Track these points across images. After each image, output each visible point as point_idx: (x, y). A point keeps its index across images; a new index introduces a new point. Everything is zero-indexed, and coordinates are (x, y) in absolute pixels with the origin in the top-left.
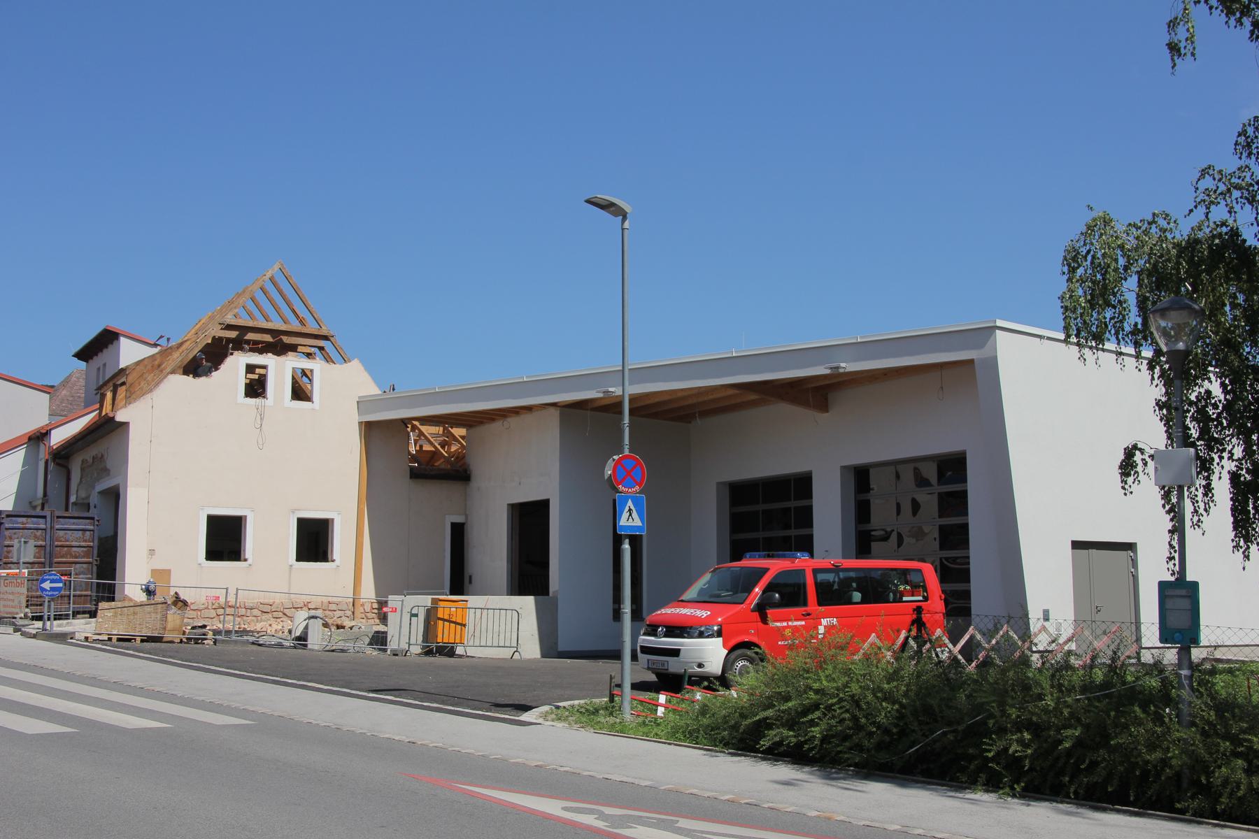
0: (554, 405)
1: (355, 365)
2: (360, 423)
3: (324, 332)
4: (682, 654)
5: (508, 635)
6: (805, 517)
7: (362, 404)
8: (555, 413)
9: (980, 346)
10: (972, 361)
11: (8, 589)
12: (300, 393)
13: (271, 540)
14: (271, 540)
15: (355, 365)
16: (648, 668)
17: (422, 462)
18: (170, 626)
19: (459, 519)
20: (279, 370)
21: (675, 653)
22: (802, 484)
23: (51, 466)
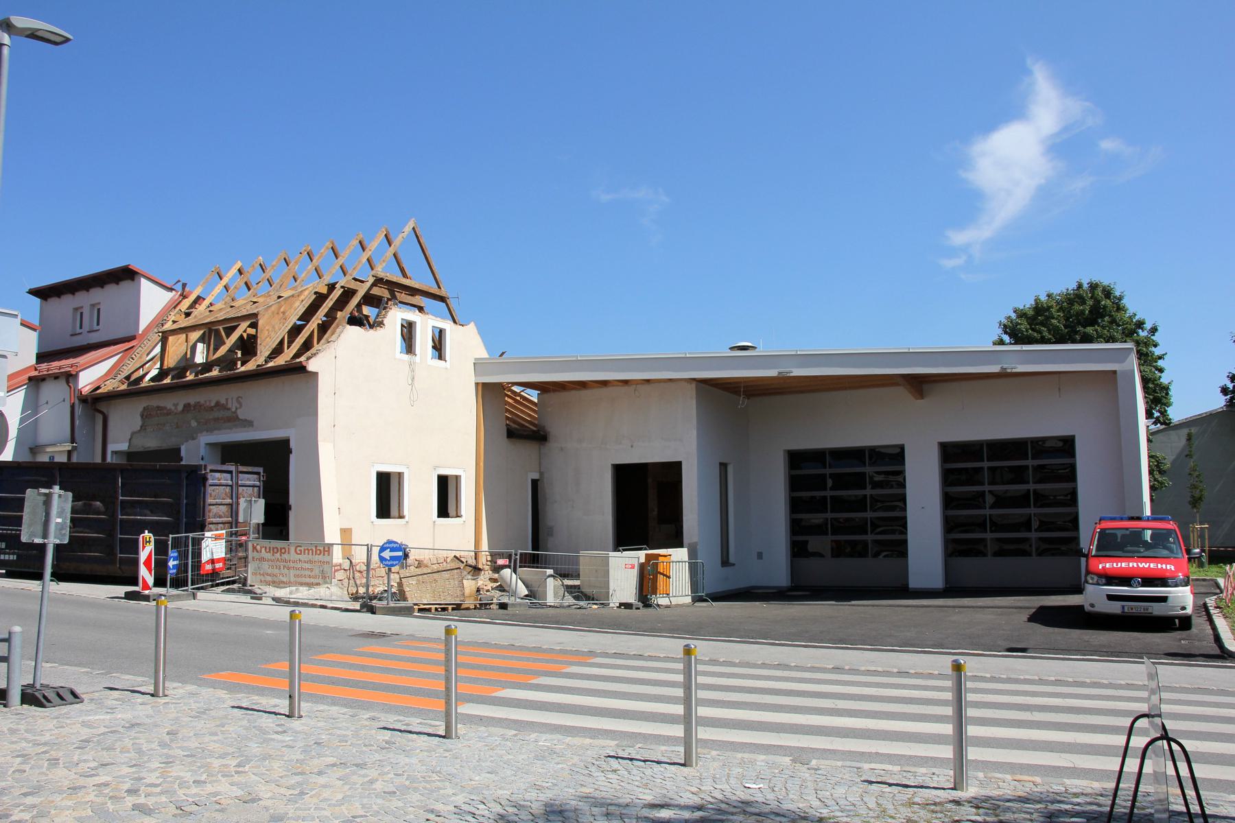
0: (694, 379)
1: (471, 328)
2: (477, 384)
3: (443, 293)
4: (1170, 600)
5: (307, 573)
6: (948, 477)
7: (478, 365)
8: (694, 385)
9: (1122, 361)
10: (1115, 372)
11: (302, 557)
12: (438, 347)
13: (419, 496)
14: (419, 496)
15: (471, 328)
16: (701, 600)
17: (521, 422)
18: (467, 592)
19: (536, 476)
20: (425, 325)
21: (1164, 599)
22: (897, 456)
23: (79, 410)
